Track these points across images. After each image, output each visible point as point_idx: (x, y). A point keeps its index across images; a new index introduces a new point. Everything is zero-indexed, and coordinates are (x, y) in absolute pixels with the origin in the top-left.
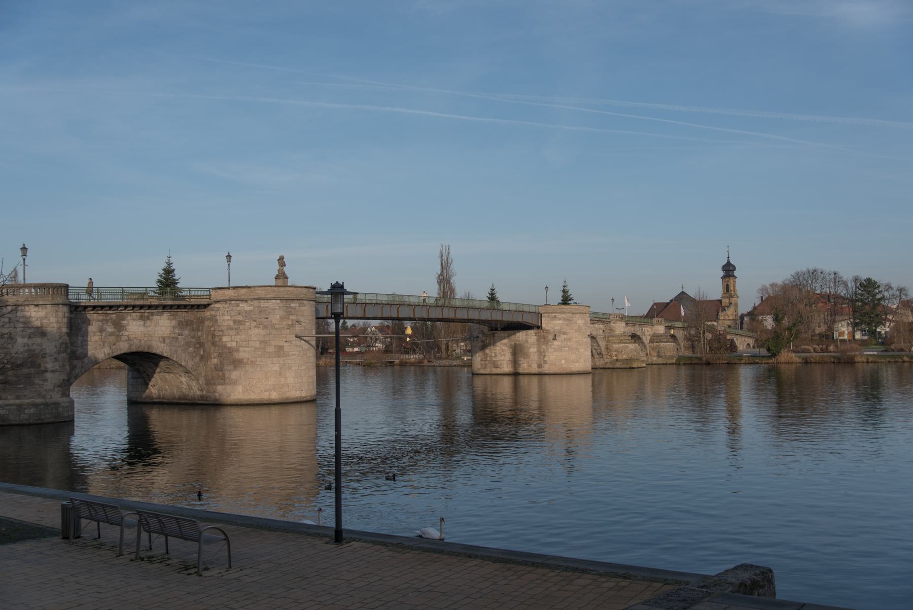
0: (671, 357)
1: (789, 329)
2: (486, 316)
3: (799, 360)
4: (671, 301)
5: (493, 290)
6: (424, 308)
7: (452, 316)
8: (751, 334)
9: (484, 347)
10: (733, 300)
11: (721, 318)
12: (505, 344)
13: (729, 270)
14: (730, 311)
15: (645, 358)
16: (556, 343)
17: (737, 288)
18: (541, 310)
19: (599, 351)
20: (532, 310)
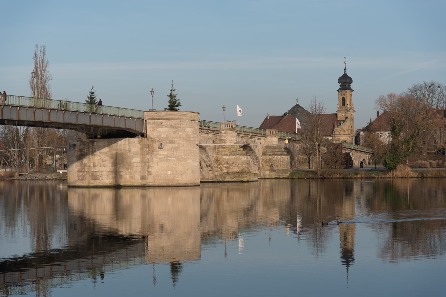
0: (285, 171)
1: (406, 142)
2: (84, 120)
3: (415, 175)
4: (285, 114)
5: (92, 93)
6: (14, 109)
7: (45, 119)
8: (366, 149)
9: (81, 157)
10: (348, 114)
11: (337, 133)
12: (105, 153)
13: (345, 82)
14: (346, 126)
15: (257, 172)
16: (161, 152)
17: (353, 102)
18: (146, 116)
19: (208, 163)
20: (136, 115)
